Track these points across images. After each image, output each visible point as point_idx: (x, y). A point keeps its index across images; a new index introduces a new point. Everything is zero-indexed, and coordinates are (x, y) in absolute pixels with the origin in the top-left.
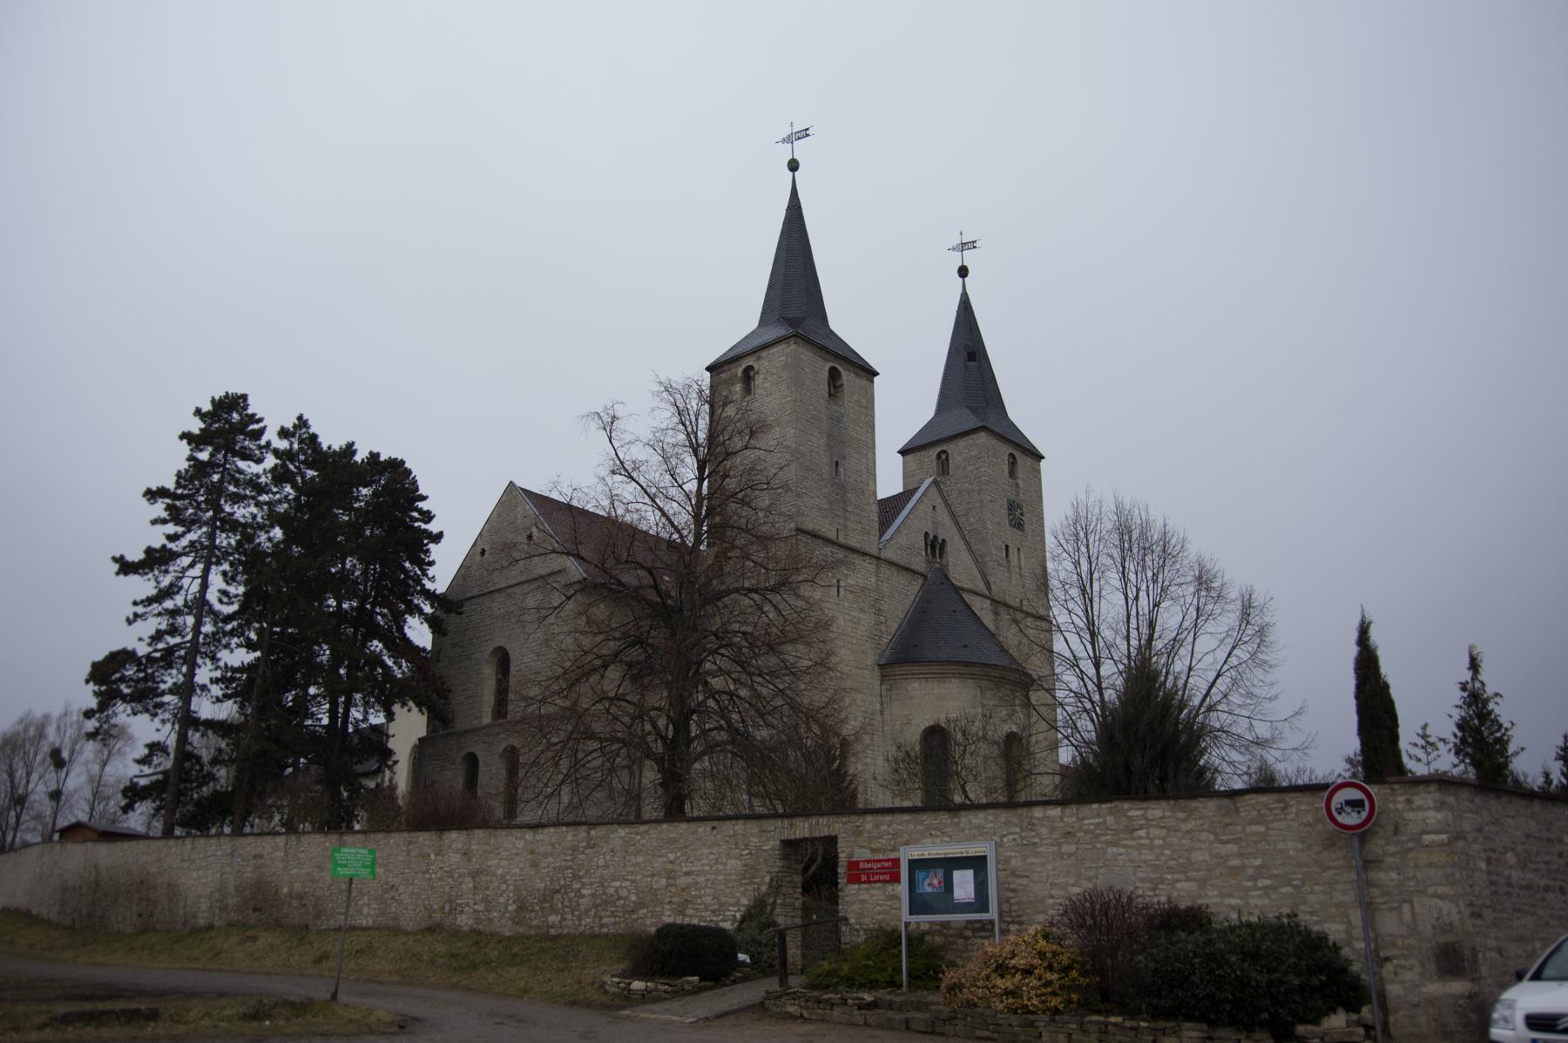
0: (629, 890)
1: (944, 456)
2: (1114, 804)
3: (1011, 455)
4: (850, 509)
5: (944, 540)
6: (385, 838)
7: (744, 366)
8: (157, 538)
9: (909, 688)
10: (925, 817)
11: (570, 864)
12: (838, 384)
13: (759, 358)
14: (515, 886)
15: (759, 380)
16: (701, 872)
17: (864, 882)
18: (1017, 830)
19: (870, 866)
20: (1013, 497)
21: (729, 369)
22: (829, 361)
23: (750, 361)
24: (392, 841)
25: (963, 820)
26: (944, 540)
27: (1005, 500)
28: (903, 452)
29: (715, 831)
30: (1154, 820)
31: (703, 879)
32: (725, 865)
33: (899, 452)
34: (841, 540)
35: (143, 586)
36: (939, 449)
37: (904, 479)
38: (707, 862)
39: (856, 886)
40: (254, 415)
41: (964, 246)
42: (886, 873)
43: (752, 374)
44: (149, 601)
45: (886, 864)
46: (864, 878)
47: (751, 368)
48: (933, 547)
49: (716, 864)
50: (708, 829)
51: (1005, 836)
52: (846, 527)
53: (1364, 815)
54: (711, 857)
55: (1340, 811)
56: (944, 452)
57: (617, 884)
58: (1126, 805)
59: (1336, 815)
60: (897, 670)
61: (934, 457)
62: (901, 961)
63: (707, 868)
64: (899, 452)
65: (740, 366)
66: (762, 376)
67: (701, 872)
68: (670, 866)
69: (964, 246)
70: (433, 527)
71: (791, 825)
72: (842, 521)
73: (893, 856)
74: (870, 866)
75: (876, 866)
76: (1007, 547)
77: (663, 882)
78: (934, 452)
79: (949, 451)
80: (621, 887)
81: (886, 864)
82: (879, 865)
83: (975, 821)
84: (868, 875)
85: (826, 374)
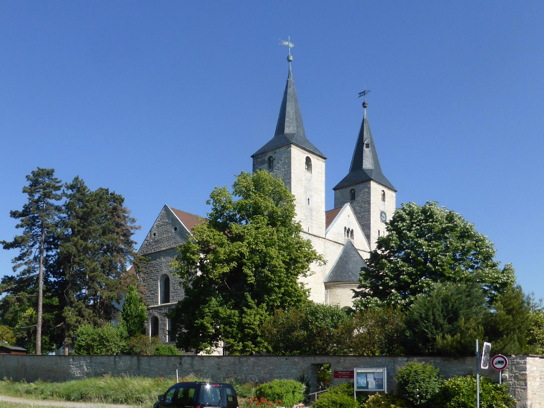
0: (256, 378)
1: (353, 191)
2: (425, 358)
3: (383, 191)
4: (313, 218)
5: (352, 230)
6: (157, 358)
7: (268, 156)
8: (20, 232)
9: (337, 292)
10: (362, 359)
11: (233, 369)
12: (309, 164)
13: (275, 153)
14: (211, 376)
15: (275, 162)
16: (282, 373)
17: (340, 378)
18: (392, 364)
19: (342, 373)
20: (382, 210)
21: (262, 157)
22: (306, 154)
23: (270, 154)
24: (160, 359)
25: (374, 360)
26: (352, 230)
27: (379, 211)
28: (335, 189)
29: (287, 360)
30: (438, 363)
31: (283, 375)
32: (291, 371)
33: (333, 189)
34: (310, 232)
35: (16, 252)
36: (351, 188)
37: (335, 201)
38: (284, 370)
39: (337, 379)
40: (56, 179)
41: (363, 93)
42: (348, 375)
43: (272, 159)
44: (20, 258)
45: (348, 373)
46: (340, 376)
47: (271, 157)
48: (348, 232)
49: (287, 370)
50: (285, 359)
51: (388, 366)
52: (312, 226)
53: (503, 366)
54: (286, 368)
55: (496, 364)
56: (353, 189)
57: (251, 376)
58: (429, 358)
59: (495, 365)
60: (334, 286)
61: (349, 190)
62: (158, 299)
63: (284, 372)
64: (333, 189)
65: (267, 156)
66: (277, 161)
67: (282, 373)
68: (270, 371)
69: (363, 93)
70: (136, 224)
71: (315, 359)
72: (310, 224)
73: (351, 370)
74: (342, 373)
75: (344, 373)
76: (379, 231)
77: (268, 376)
78: (349, 189)
79: (355, 190)
80: (252, 377)
81: (348, 373)
82: (345, 373)
83: (379, 361)
84: (341, 375)
85: (304, 161)
